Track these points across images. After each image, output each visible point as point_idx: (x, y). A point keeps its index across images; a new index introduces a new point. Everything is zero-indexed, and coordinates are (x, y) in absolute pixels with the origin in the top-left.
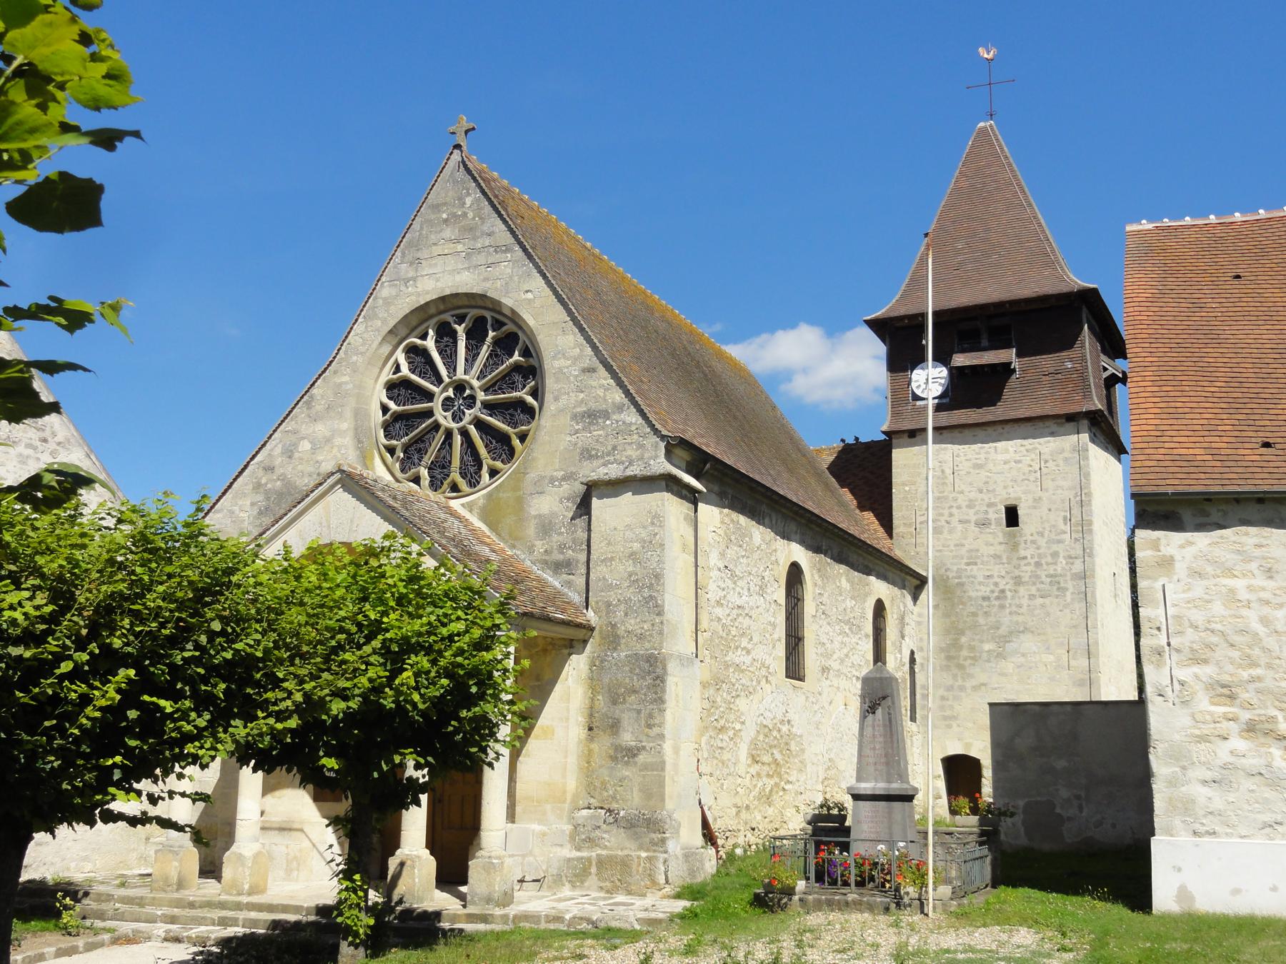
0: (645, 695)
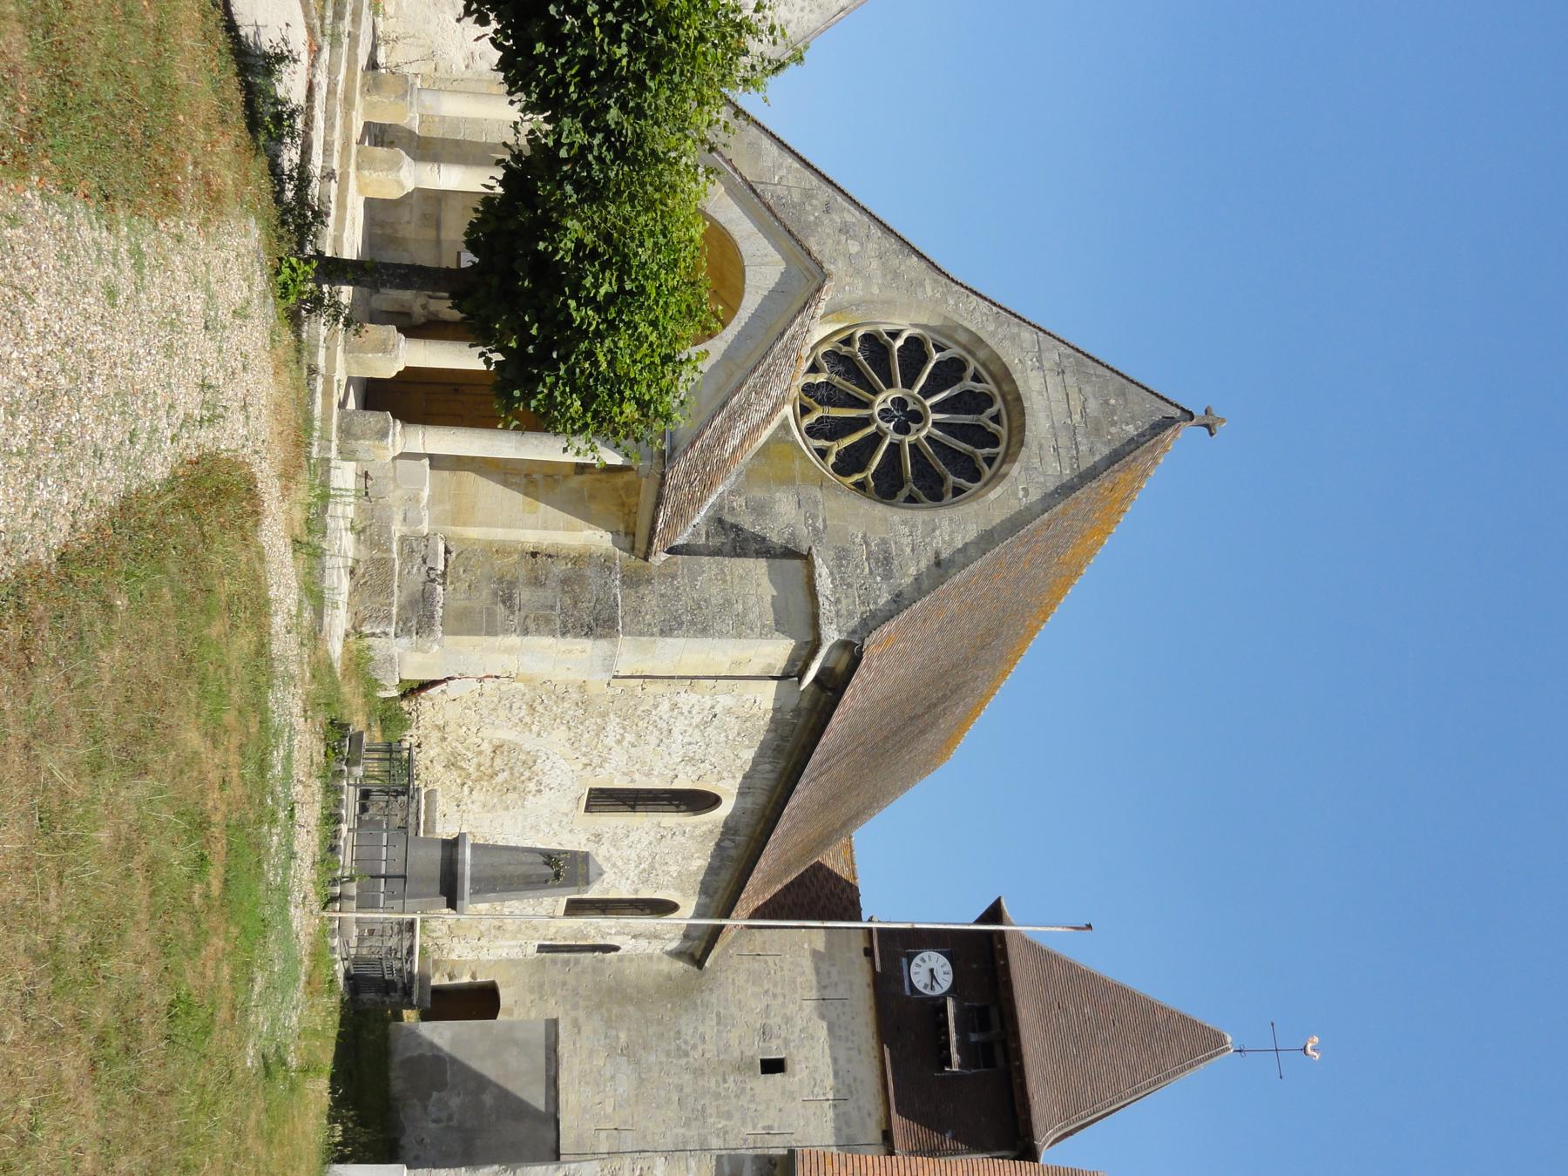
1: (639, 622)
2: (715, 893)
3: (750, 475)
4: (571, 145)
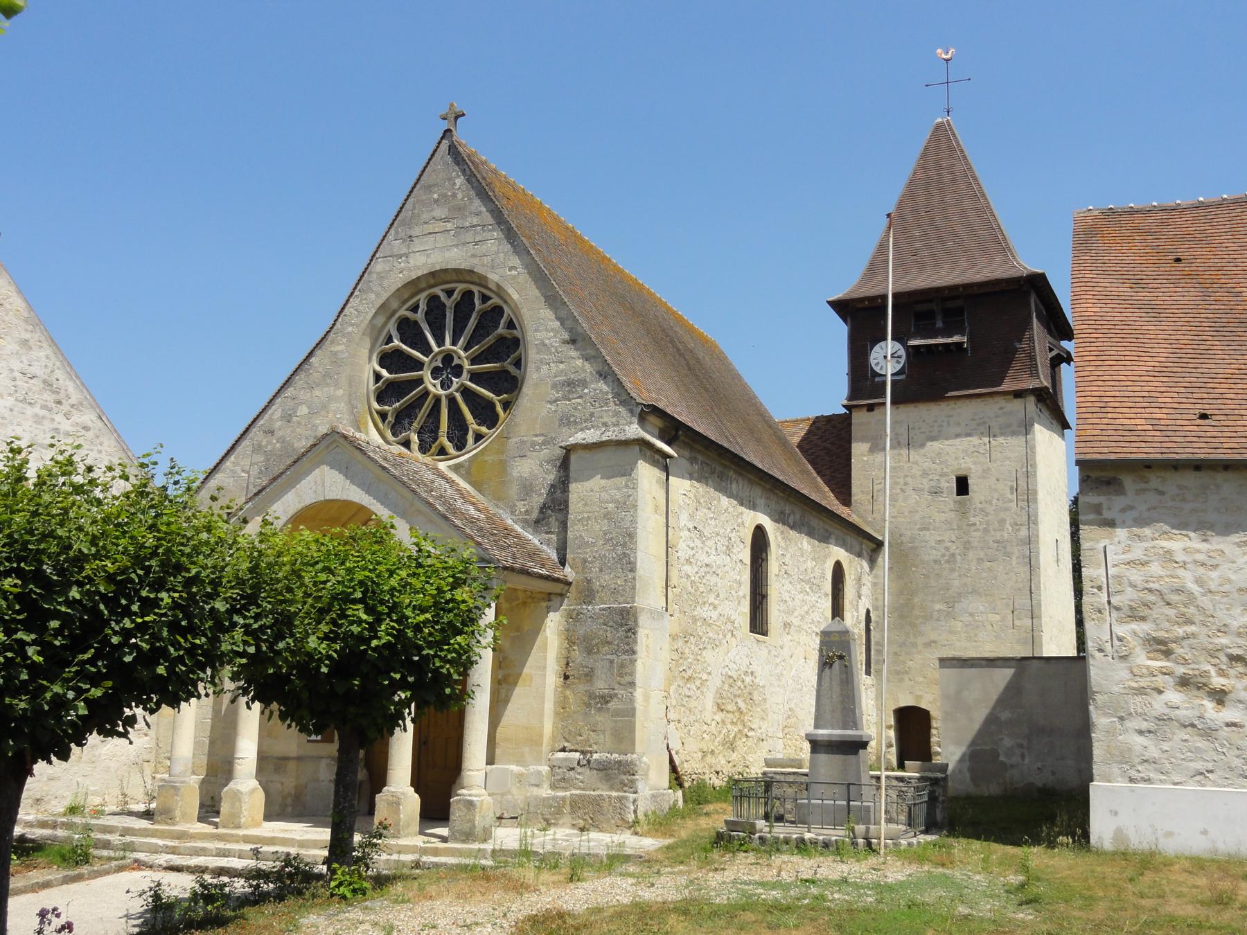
1: (623, 590)
2: (827, 531)
3: (498, 498)
4: (245, 643)
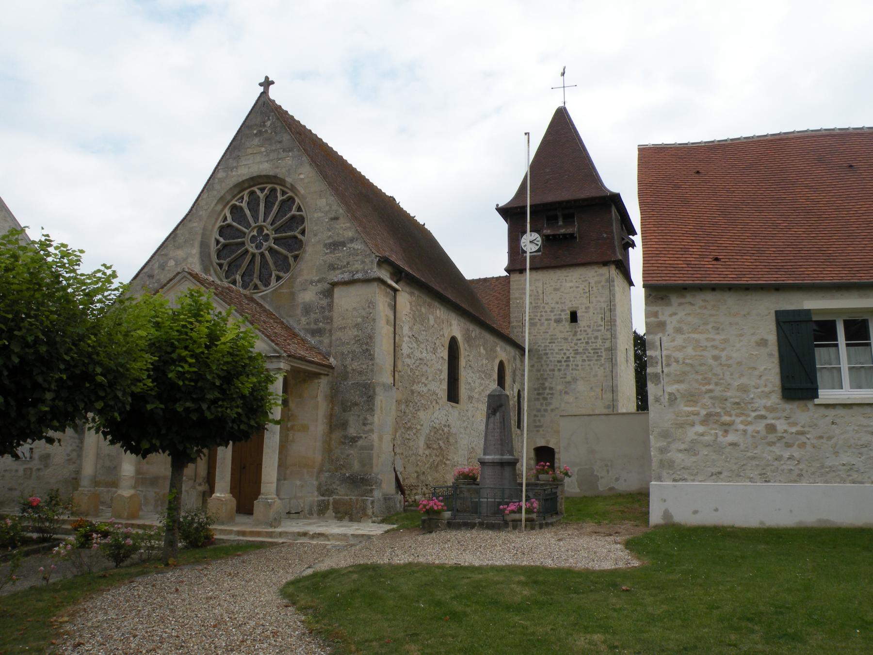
0: (362, 406)
1: (367, 372)
